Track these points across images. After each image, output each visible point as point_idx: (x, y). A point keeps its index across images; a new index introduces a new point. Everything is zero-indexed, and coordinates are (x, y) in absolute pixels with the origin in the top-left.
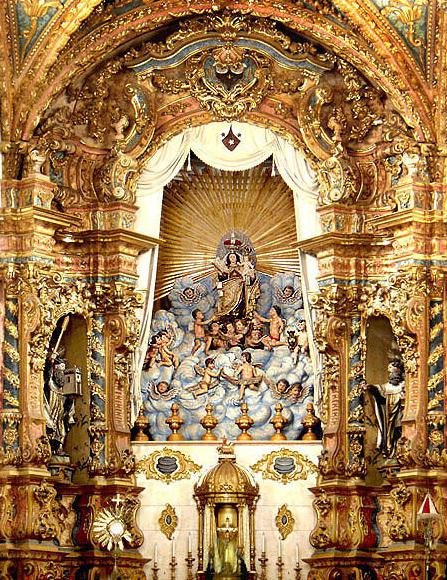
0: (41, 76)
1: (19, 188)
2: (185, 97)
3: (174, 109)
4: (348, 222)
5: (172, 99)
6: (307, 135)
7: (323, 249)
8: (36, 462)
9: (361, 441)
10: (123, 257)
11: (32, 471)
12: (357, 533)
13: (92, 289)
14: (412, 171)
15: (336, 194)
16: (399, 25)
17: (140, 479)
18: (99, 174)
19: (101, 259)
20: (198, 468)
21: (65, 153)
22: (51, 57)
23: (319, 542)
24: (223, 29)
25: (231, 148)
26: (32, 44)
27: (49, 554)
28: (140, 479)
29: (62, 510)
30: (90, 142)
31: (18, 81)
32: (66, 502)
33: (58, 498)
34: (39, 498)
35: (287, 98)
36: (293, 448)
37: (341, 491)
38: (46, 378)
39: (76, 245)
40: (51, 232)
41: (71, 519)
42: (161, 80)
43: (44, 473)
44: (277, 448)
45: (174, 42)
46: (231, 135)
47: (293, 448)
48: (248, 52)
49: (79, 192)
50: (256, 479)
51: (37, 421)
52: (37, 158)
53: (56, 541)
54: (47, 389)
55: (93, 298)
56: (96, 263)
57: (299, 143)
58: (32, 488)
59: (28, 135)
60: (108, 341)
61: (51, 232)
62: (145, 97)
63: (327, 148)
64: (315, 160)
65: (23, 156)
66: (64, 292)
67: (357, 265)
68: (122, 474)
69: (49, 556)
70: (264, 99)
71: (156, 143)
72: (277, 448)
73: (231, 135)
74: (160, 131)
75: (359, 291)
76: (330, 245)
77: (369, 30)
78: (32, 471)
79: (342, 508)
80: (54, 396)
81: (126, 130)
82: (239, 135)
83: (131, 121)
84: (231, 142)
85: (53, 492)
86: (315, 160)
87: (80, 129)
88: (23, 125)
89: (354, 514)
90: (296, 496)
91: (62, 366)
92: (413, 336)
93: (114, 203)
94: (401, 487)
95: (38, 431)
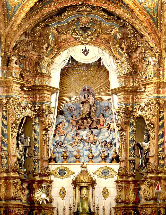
0: (15, 28)
1: (7, 70)
2: (69, 36)
3: (64, 40)
4: (129, 82)
5: (64, 37)
6: (114, 50)
7: (120, 92)
8: (14, 171)
9: (134, 163)
10: (46, 95)
11: (12, 174)
12: (132, 197)
13: (34, 107)
14: (153, 63)
15: (124, 72)
16: (148, 9)
17: (52, 178)
18: (37, 64)
19: (38, 96)
20: (73, 173)
21: (24, 56)
22: (19, 21)
23: (118, 201)
24: (83, 11)
25: (86, 55)
26: (12, 16)
27: (19, 205)
28: (52, 178)
29: (23, 189)
30: (34, 53)
31: (7, 30)
32: (25, 186)
33: (22, 184)
34: (15, 185)
35: (106, 36)
36: (108, 166)
37: (127, 182)
38: (17, 140)
39: (29, 91)
40: (19, 86)
41: (27, 192)
42: (60, 30)
43: (17, 175)
44: (103, 166)
45: (65, 15)
46: (85, 50)
47: (108, 166)
48: (92, 19)
49: (29, 71)
50: (95, 177)
51: (14, 156)
52: (14, 58)
53: (21, 200)
54: (18, 144)
55: (35, 110)
56: (36, 98)
57: (111, 53)
58: (12, 181)
59: (11, 50)
60: (40, 126)
61: (19, 86)
62: (54, 36)
63: (121, 55)
64: (117, 59)
65: (9, 58)
66: (24, 108)
67: (132, 98)
68: (45, 175)
69: (18, 206)
70: (98, 37)
71: (58, 53)
72: (103, 166)
73: (85, 50)
74: (59, 49)
75: (133, 108)
76: (122, 91)
77: (137, 11)
78: (12, 174)
79: (127, 188)
80: (20, 147)
81: (47, 48)
82: (89, 50)
83: (49, 45)
84: (86, 53)
85: (20, 182)
86: (117, 59)
87: (30, 48)
88: (9, 46)
89: (131, 191)
90: (109, 184)
91: (23, 136)
92: (153, 124)
93: (42, 75)
94: (149, 180)
95: (14, 160)
